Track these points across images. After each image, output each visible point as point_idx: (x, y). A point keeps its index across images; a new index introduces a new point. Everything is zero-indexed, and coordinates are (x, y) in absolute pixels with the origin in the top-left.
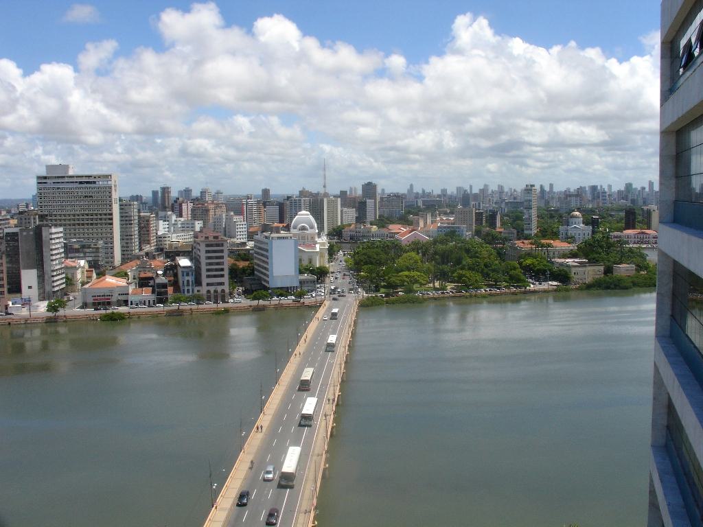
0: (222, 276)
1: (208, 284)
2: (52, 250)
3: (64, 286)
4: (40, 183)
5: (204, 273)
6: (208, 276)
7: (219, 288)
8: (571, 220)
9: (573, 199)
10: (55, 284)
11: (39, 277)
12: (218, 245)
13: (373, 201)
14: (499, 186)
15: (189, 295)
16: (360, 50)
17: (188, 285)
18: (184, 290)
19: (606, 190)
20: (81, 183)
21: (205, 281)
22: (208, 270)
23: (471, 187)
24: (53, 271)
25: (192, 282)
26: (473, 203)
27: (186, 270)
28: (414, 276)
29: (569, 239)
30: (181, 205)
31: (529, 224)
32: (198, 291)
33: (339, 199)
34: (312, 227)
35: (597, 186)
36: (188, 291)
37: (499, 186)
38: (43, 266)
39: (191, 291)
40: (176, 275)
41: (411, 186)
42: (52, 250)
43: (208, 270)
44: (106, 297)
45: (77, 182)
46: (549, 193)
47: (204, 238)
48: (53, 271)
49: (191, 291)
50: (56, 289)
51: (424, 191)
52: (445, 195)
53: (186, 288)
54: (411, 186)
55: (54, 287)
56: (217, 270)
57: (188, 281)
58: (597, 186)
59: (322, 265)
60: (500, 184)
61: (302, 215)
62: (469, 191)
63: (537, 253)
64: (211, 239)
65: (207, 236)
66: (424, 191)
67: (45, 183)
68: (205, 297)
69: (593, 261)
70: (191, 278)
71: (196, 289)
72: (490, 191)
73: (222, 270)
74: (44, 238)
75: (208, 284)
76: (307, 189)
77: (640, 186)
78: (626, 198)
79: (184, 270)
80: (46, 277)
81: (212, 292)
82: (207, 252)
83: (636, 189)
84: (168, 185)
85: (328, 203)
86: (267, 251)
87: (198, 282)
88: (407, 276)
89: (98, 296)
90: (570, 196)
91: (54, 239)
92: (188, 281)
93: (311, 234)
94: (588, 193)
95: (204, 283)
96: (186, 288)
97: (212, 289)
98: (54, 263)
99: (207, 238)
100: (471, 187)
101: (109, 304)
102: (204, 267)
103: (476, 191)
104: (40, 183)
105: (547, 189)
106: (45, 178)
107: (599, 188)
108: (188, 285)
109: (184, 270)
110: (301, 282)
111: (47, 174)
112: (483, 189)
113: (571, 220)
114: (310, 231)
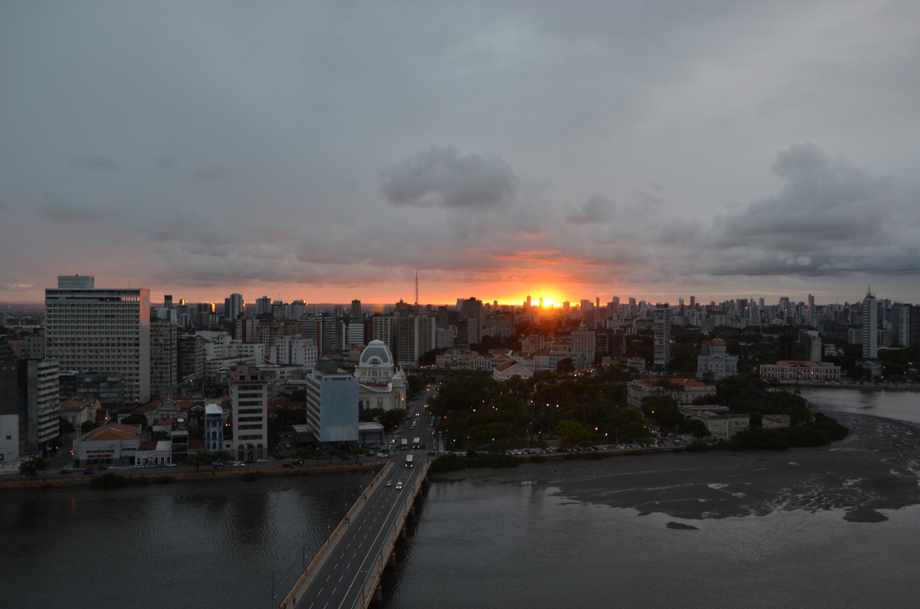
0: (260, 427)
2: (40, 390)
3: (57, 434)
4: (51, 298)
5: (236, 423)
6: (241, 427)
7: (255, 443)
8: (712, 348)
9: (718, 317)
10: (42, 434)
11: (20, 424)
12: (254, 388)
13: (475, 320)
15: (214, 450)
16: (4, 327)
19: (758, 304)
20: (101, 299)
21: (237, 432)
22: (241, 420)
24: (40, 417)
25: (220, 433)
29: (708, 379)
30: (244, 322)
32: (228, 446)
35: (747, 300)
38: (27, 410)
39: (217, 445)
40: (201, 423)
42: (40, 390)
43: (241, 420)
44: (105, 453)
45: (96, 298)
46: (689, 307)
47: (238, 378)
48: (40, 417)
49: (217, 445)
50: (43, 440)
53: (212, 443)
55: (41, 437)
56: (252, 419)
58: (747, 300)
59: (397, 407)
61: (374, 345)
65: (242, 375)
67: (57, 298)
68: (236, 455)
69: (737, 410)
70: (217, 429)
71: (225, 443)
74: (29, 375)
76: (404, 302)
77: (799, 301)
78: (781, 316)
79: (210, 418)
80: (30, 425)
83: (793, 303)
85: (420, 322)
87: (228, 434)
89: (94, 452)
90: (714, 313)
91: (44, 375)
92: (214, 433)
93: (384, 369)
94: (736, 307)
95: (235, 437)
97: (244, 443)
98: (43, 406)
101: (109, 461)
102: (236, 416)
104: (51, 298)
105: (687, 303)
106: (56, 292)
107: (749, 301)
109: (210, 418)
110: (363, 434)
111: (59, 287)
113: (712, 348)
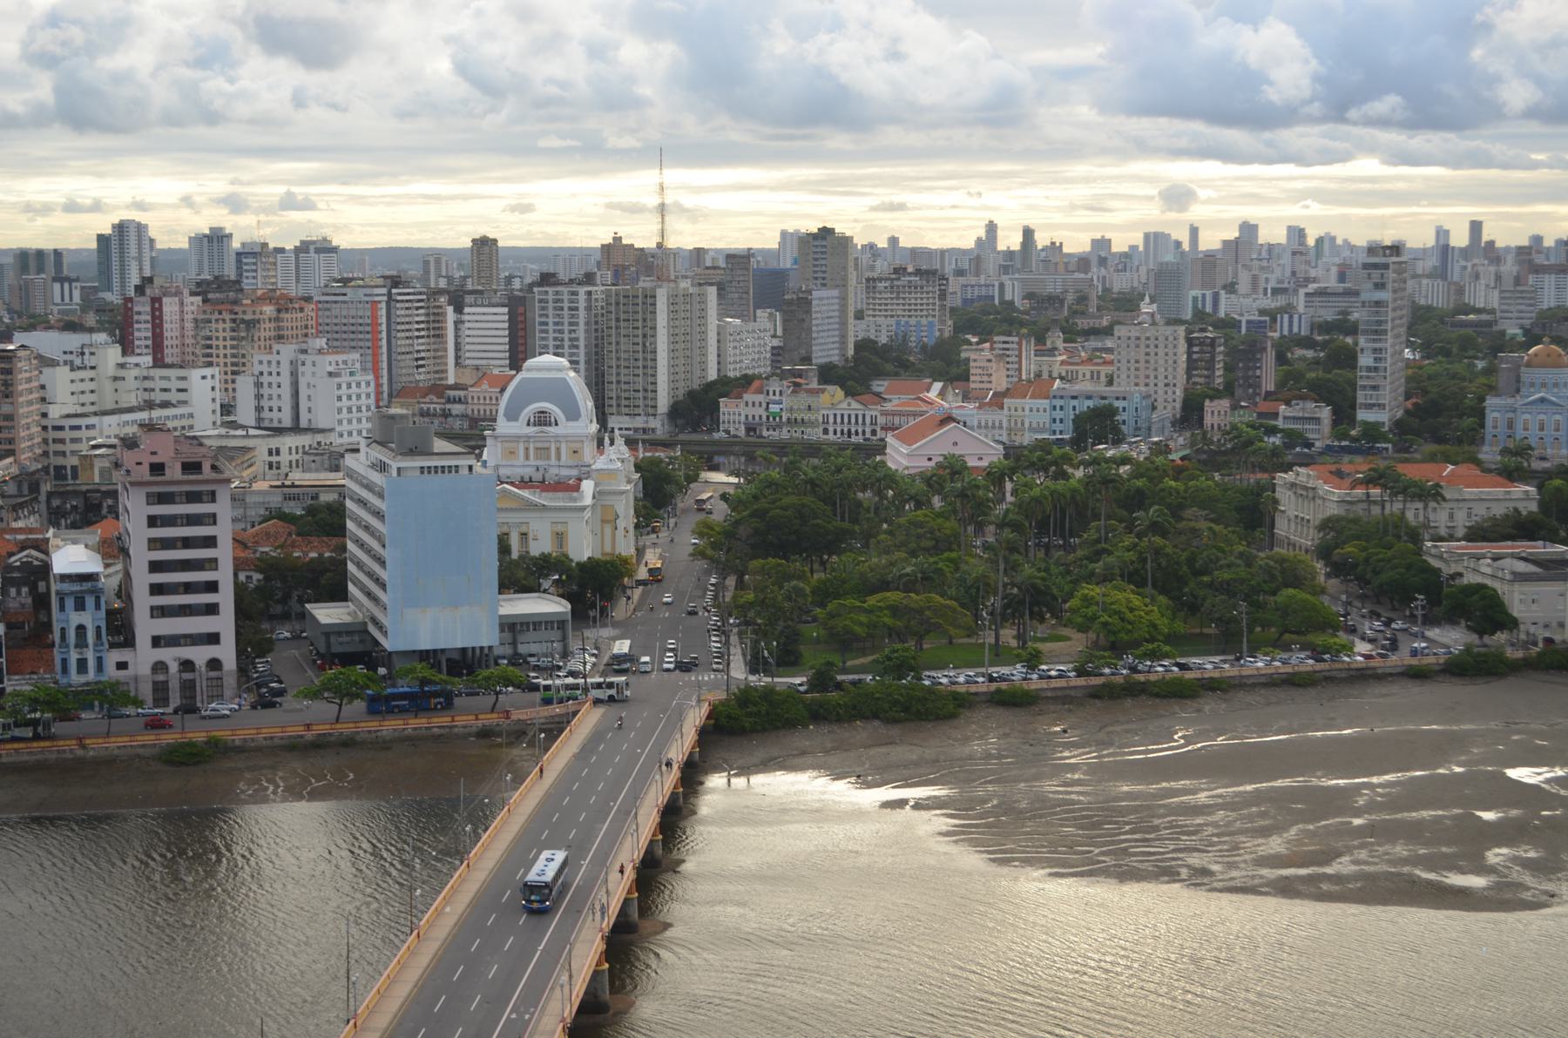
0: (212, 609)
1: (157, 642)
5: (143, 601)
6: (160, 612)
7: (200, 655)
12: (193, 497)
13: (835, 293)
14: (1290, 228)
15: (83, 679)
17: (81, 643)
18: (64, 661)
21: (145, 627)
23: (1194, 232)
26: (1193, 293)
27: (76, 587)
28: (920, 611)
31: (1375, 388)
32: (122, 666)
33: (712, 292)
34: (573, 414)
36: (82, 665)
37: (1290, 228)
39: (91, 664)
41: (992, 228)
43: (156, 589)
47: (146, 468)
49: (91, 664)
51: (894, 241)
52: (1103, 261)
53: (74, 656)
54: (992, 228)
57: (81, 629)
60: (1026, 223)
62: (1186, 246)
63: (1421, 518)
64: (174, 472)
65: (156, 459)
66: (894, 241)
70: (90, 618)
72: (1311, 242)
73: (212, 587)
75: (157, 642)
81: (174, 668)
82: (153, 521)
84: (1541, 234)
85: (673, 303)
86: (426, 263)
88: (895, 610)
90: (1538, 270)
96: (74, 656)
97: (169, 655)
99: (157, 468)
100: (1194, 232)
103: (1211, 241)
108: (81, 643)
112: (1237, 241)
114: (565, 428)
